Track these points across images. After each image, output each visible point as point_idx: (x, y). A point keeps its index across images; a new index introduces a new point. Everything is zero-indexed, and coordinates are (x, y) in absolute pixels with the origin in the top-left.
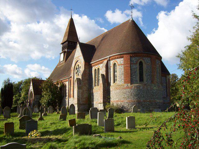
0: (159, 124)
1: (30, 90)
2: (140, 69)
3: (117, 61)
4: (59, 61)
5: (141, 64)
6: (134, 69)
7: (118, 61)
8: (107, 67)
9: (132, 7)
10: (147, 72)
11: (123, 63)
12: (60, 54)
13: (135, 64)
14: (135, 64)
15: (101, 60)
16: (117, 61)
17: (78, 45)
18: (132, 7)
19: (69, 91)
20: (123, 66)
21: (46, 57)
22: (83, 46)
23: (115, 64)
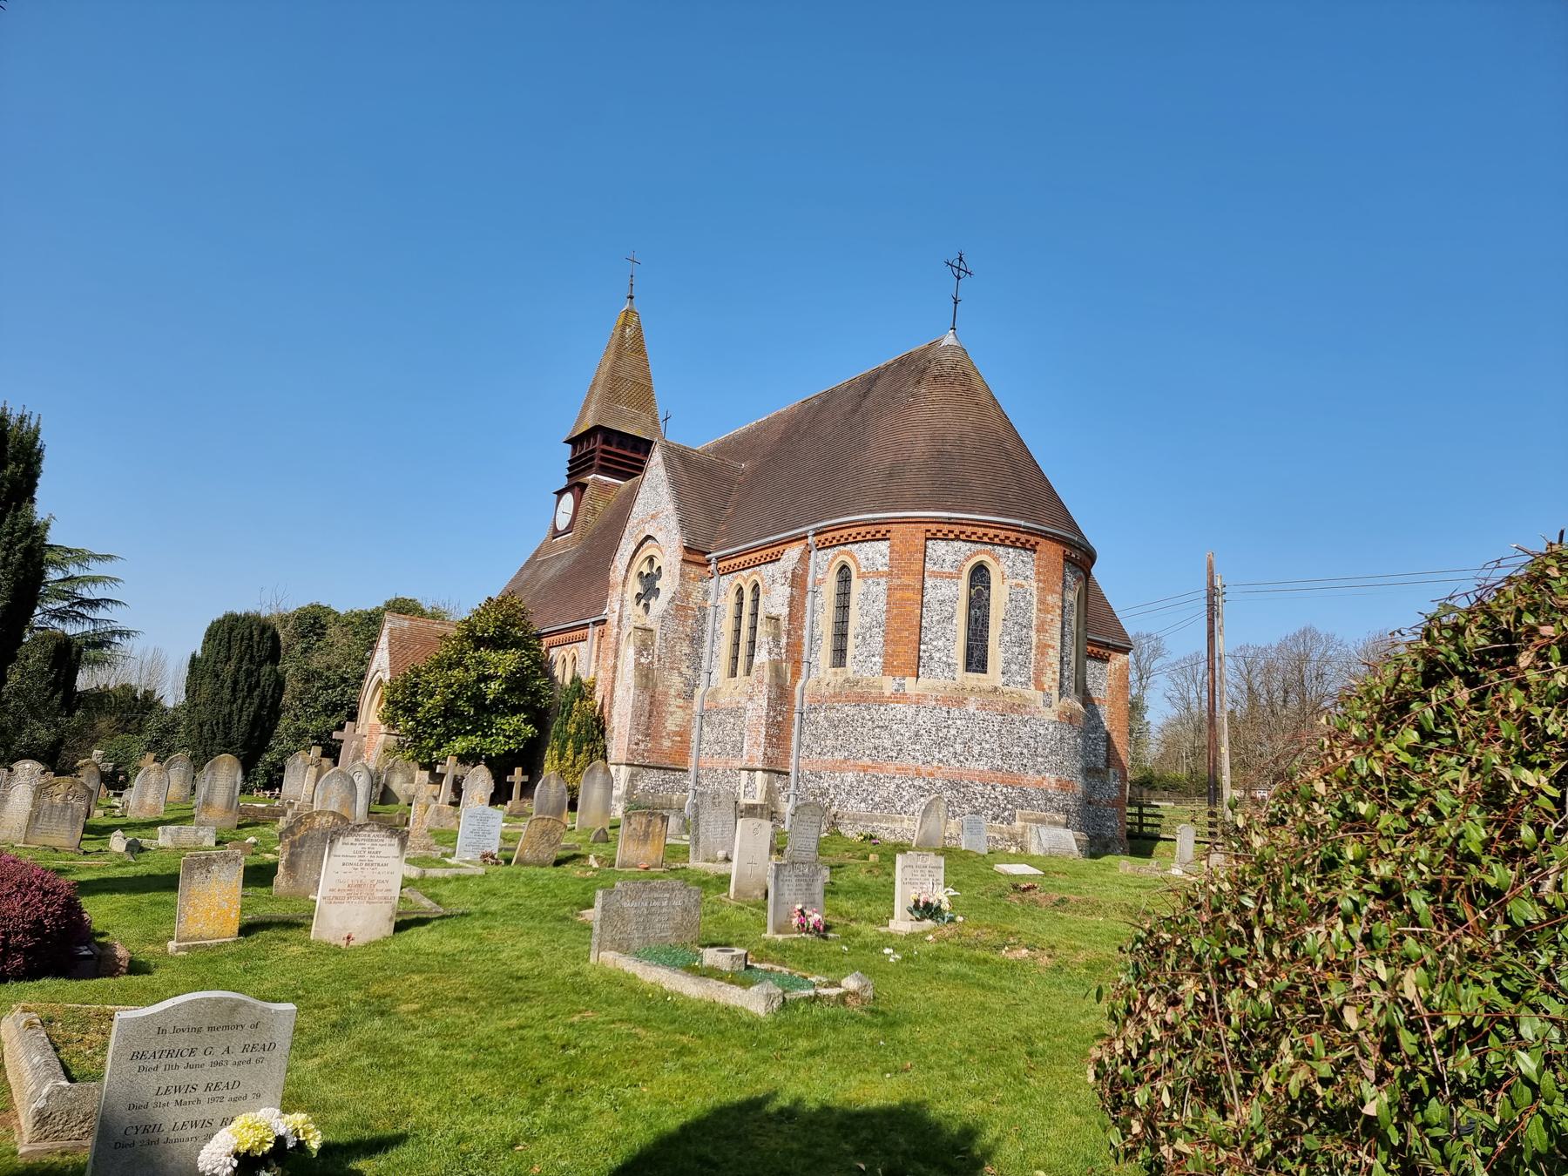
0: (1077, 1114)
1: (373, 669)
2: (971, 605)
3: (853, 557)
4: (547, 532)
5: (980, 573)
6: (942, 602)
7: (861, 557)
8: (797, 580)
9: (962, 274)
10: (1010, 624)
11: (886, 569)
12: (560, 493)
13: (950, 576)
14: (950, 576)
15: (773, 545)
16: (853, 557)
17: (656, 458)
18: (962, 274)
19: (752, 643)
20: (883, 581)
21: (1560, 657)
22: (681, 460)
23: (844, 574)
